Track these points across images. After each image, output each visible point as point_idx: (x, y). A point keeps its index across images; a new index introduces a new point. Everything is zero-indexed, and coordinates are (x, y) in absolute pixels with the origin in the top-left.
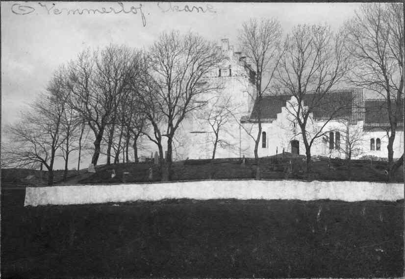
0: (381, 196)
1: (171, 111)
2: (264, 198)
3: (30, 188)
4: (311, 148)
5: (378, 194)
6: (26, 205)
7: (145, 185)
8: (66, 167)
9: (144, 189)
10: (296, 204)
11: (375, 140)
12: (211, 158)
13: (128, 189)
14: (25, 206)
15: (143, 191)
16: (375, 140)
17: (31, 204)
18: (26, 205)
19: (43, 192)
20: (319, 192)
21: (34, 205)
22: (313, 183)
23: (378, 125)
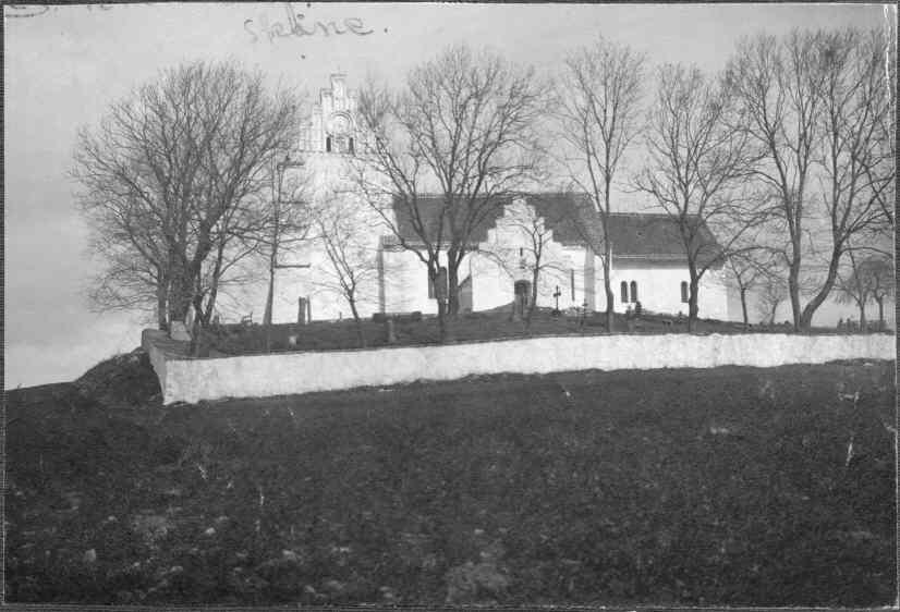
0: (804, 357)
1: (208, 249)
2: (639, 367)
3: (178, 362)
4: (700, 281)
5: (799, 355)
6: (168, 400)
7: (429, 350)
8: (355, 313)
9: (427, 357)
10: (362, 397)
11: (629, 284)
12: (295, 320)
13: (395, 359)
14: (165, 403)
15: (425, 362)
16: (629, 284)
17: (181, 399)
18: (168, 400)
19: (210, 371)
20: (719, 353)
21: (192, 399)
22: (711, 337)
23: (208, 297)
